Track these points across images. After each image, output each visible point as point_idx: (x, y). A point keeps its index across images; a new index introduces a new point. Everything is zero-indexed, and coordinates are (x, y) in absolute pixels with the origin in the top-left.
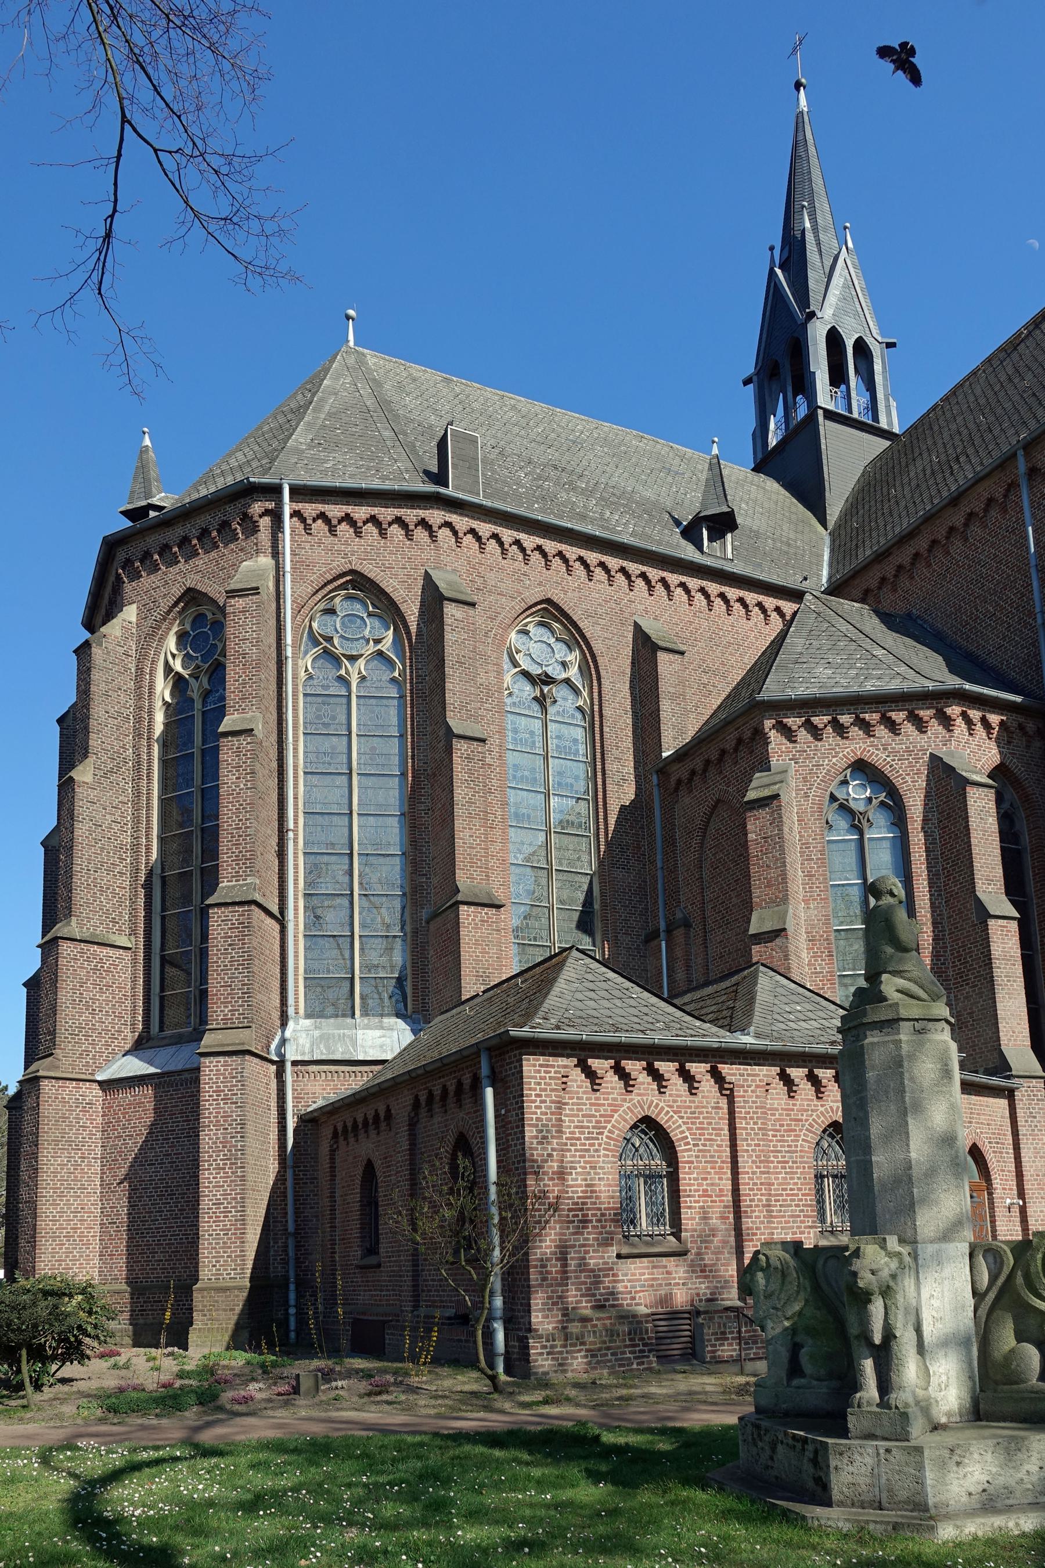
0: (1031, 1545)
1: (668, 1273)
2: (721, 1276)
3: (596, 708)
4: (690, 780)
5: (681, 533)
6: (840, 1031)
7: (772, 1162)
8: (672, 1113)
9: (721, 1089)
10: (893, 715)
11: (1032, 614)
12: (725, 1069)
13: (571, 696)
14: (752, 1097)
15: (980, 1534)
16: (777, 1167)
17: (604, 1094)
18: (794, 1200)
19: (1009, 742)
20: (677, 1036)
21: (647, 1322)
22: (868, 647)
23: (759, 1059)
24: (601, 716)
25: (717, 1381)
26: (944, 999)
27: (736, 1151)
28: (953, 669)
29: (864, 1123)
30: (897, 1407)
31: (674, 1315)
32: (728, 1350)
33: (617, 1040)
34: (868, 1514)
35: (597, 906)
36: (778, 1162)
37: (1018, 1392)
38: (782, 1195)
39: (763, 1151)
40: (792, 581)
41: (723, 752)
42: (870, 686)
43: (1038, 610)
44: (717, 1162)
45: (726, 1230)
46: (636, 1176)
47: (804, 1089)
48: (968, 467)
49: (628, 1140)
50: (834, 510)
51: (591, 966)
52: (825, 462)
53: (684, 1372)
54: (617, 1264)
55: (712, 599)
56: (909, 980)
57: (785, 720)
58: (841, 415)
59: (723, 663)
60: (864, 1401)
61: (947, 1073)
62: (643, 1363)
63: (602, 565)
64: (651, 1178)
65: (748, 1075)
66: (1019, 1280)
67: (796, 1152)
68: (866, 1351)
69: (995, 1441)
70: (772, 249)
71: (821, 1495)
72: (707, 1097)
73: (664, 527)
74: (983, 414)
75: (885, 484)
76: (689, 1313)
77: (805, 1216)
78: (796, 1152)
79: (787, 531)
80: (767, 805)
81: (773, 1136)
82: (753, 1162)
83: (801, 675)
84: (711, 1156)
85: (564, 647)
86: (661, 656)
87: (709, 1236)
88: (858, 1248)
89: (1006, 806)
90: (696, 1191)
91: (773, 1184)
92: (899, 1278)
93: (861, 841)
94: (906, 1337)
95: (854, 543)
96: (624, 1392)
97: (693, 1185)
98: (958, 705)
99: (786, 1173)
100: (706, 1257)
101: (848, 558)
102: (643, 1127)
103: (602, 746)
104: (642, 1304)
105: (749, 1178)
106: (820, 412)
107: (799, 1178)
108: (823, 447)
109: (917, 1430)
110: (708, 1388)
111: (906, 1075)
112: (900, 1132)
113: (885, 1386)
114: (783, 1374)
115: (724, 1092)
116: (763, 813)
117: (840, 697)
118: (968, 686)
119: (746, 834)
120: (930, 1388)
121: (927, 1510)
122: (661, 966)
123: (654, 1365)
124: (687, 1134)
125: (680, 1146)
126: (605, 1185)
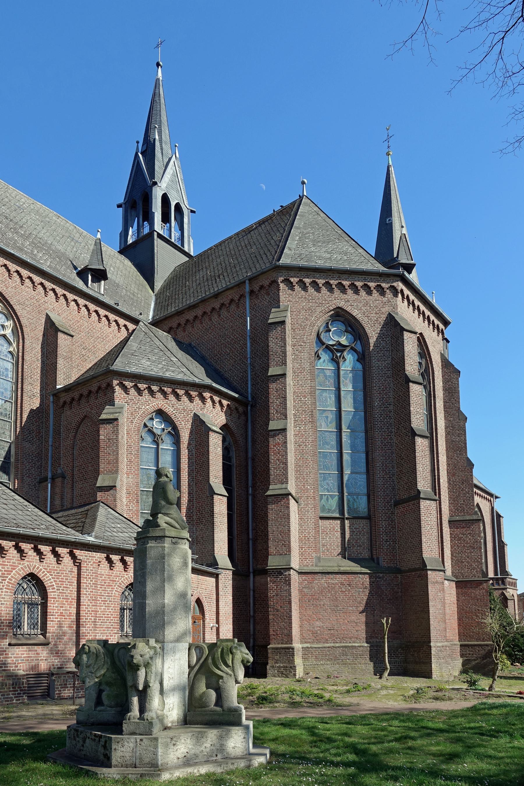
0: (203, 779)
1: (37, 654)
2: (66, 656)
3: (20, 354)
4: (71, 402)
5: (77, 273)
6: (136, 539)
7: (99, 601)
8: (46, 572)
9: (74, 562)
10: (178, 391)
11: (246, 358)
12: (77, 552)
13: (6, 345)
14: (90, 567)
15: (181, 776)
16: (101, 603)
17: (7, 559)
18: (108, 620)
19: (231, 415)
20: (52, 533)
21: (23, 679)
22: (169, 355)
23: (96, 549)
24: (23, 359)
25: (60, 708)
26: (187, 529)
27: (80, 594)
28: (208, 375)
29: (143, 584)
30: (147, 720)
31: (39, 675)
32: (67, 693)
33: (18, 532)
34: (129, 770)
35: (12, 460)
36: (102, 601)
37: (205, 711)
38: (102, 617)
39: (94, 595)
40: (134, 314)
41: (90, 392)
42: (168, 375)
43: (249, 356)
44: (69, 599)
45: (72, 633)
46: (23, 603)
47: (118, 566)
48: (223, 281)
49: (20, 585)
50: (159, 284)
51: (6, 491)
52: (156, 259)
53: (42, 704)
54: (8, 648)
55: (111, 322)
56: (172, 518)
57: (124, 382)
58: (166, 238)
59: (94, 346)
60: (132, 717)
61: (185, 564)
62: (19, 700)
63: (96, 312)
64: (31, 605)
65: (89, 556)
66: (210, 661)
67: (112, 596)
68: (134, 693)
69: (192, 734)
70: (138, 142)
71: (106, 762)
72: (67, 566)
73: (68, 268)
74: (233, 259)
75: (184, 278)
76: (48, 674)
77: (113, 628)
78: (112, 596)
79: (133, 288)
80: (111, 423)
81: (100, 588)
82: (89, 600)
83: (134, 361)
84: (66, 596)
85: (4, 317)
86: (60, 335)
87: (62, 636)
88: (135, 644)
89: (226, 444)
90: (56, 613)
91: (98, 611)
92: (154, 658)
93: (157, 449)
94: (155, 686)
95: (167, 303)
96: (7, 715)
97: (55, 610)
98: (209, 392)
99: (105, 606)
100: (59, 646)
101: (163, 310)
102: (29, 578)
103: (22, 375)
104: (22, 669)
105: (86, 608)
106: (155, 233)
107: (112, 609)
108: (155, 251)
109: (156, 730)
110: (55, 712)
111: (166, 563)
112: (162, 590)
113: (142, 710)
114: (93, 705)
115: (76, 564)
116: (109, 427)
117: (152, 377)
118: (214, 385)
119: (99, 436)
120: (165, 710)
121: (158, 767)
122: (47, 496)
123: (26, 701)
124: (54, 583)
125: (50, 589)
126: (4, 607)
